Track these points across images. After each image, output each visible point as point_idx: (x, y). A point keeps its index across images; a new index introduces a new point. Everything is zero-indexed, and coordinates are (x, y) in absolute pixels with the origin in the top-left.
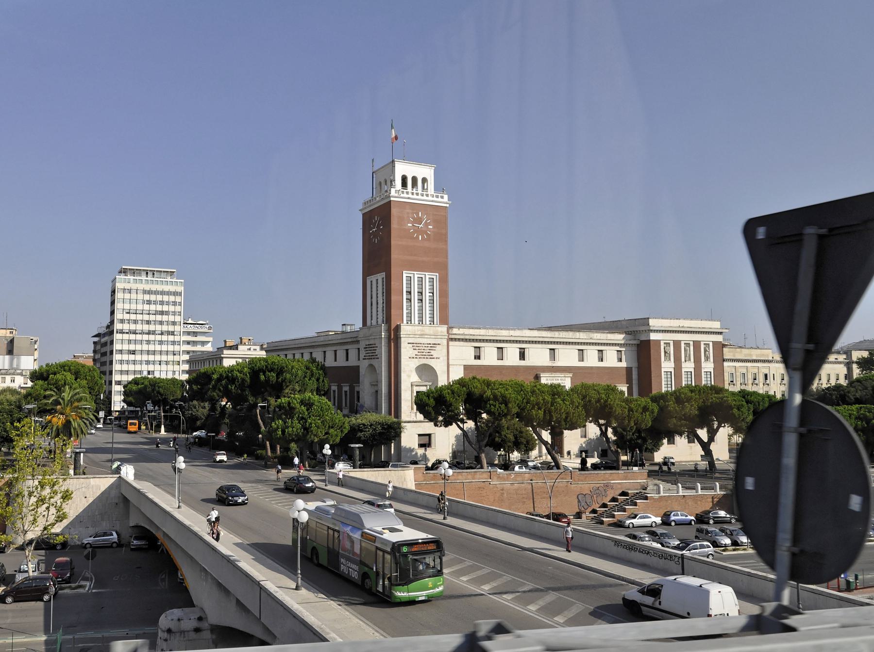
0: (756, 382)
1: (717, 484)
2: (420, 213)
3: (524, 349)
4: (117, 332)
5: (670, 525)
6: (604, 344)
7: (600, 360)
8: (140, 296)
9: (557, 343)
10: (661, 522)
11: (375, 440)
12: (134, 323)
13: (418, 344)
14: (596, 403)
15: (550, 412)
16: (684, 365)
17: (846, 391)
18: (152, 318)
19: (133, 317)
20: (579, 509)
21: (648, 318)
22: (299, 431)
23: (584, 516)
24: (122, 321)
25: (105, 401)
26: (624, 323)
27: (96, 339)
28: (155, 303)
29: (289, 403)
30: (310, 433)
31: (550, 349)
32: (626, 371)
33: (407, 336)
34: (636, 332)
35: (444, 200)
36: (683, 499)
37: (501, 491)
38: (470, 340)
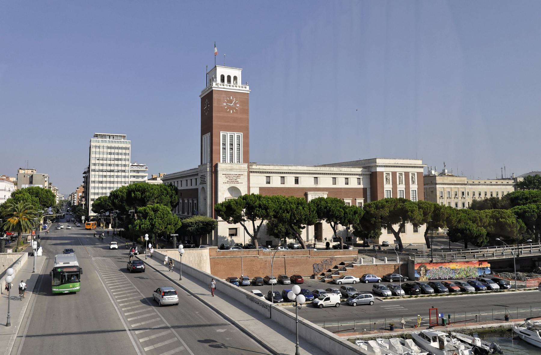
0: (457, 196)
1: (386, 258)
2: (231, 97)
3: (298, 177)
4: (92, 171)
5: (365, 282)
6: (349, 174)
7: (359, 184)
8: (105, 150)
9: (319, 174)
10: (359, 281)
11: (199, 231)
12: (101, 166)
13: (229, 174)
15: (294, 215)
16: (398, 186)
17: (497, 201)
18: (112, 162)
19: (101, 162)
20: (314, 273)
21: (376, 159)
22: (148, 227)
23: (316, 277)
24: (95, 164)
25: (85, 210)
27: (84, 175)
28: (114, 154)
29: (145, 210)
30: (155, 228)
31: (315, 177)
32: (363, 190)
33: (222, 170)
34: (369, 167)
35: (247, 89)
36: (376, 267)
37: (265, 262)
38: (263, 172)
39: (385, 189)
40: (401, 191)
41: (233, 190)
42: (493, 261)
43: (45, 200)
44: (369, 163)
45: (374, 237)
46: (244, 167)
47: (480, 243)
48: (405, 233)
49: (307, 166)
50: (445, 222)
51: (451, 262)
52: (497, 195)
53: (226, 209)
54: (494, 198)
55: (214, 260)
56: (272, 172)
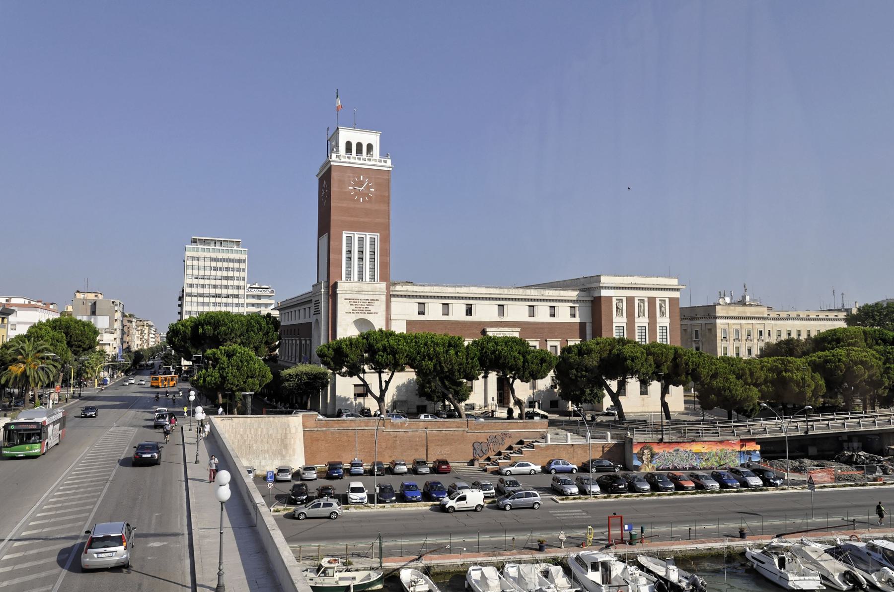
1: (609, 433)
3: (471, 305)
4: (187, 296)
6: (556, 301)
8: (208, 264)
9: (506, 299)
11: (301, 389)
12: (202, 287)
14: (491, 354)
15: (440, 363)
16: (637, 320)
18: (219, 282)
19: (201, 282)
21: (600, 276)
23: (476, 463)
24: (191, 286)
26: (582, 280)
28: (221, 269)
31: (499, 305)
33: (344, 292)
38: (413, 297)
39: (614, 325)
40: (642, 328)
41: (360, 323)
42: (765, 441)
43: (80, 338)
44: (590, 283)
45: (591, 400)
46: (380, 288)
47: (749, 410)
48: (647, 394)
49: (486, 287)
50: (689, 377)
51: (693, 441)
52: (799, 335)
53: (335, 354)
54: (792, 339)
55: (311, 434)
56: (427, 296)
